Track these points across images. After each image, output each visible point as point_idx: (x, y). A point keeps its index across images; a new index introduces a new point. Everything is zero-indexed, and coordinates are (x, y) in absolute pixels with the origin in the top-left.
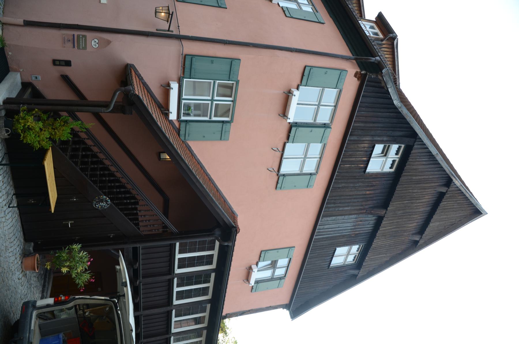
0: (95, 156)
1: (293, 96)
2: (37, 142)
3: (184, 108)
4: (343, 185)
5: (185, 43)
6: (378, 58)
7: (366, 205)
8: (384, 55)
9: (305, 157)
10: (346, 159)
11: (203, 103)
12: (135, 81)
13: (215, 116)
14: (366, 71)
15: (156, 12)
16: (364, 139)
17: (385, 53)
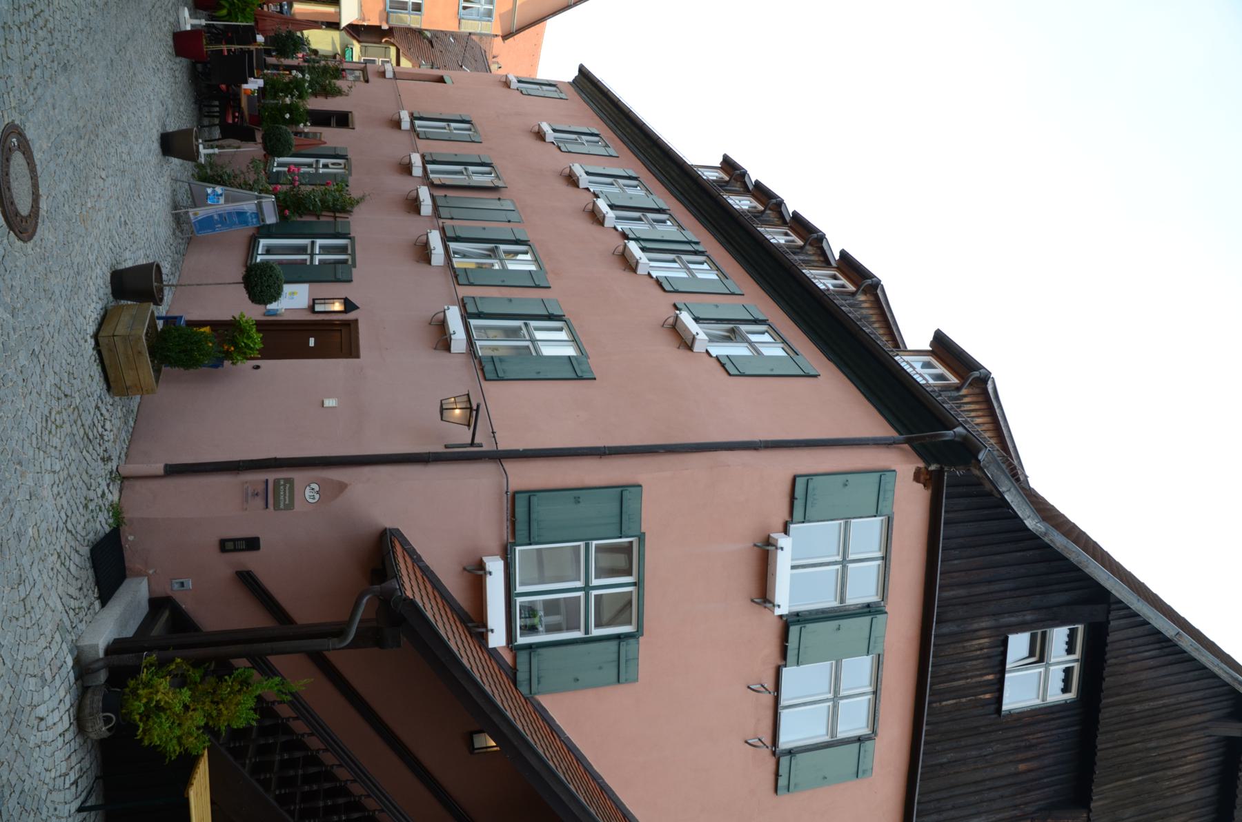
0: (313, 760)
1: (779, 551)
2: (175, 741)
3: (522, 617)
4: (951, 756)
5: (511, 467)
6: (959, 430)
7: (1026, 804)
8: (972, 421)
9: (836, 698)
10: (942, 686)
11: (565, 599)
12: (404, 566)
13: (597, 626)
14: (937, 462)
15: (442, 410)
16: (975, 626)
17: (973, 414)
